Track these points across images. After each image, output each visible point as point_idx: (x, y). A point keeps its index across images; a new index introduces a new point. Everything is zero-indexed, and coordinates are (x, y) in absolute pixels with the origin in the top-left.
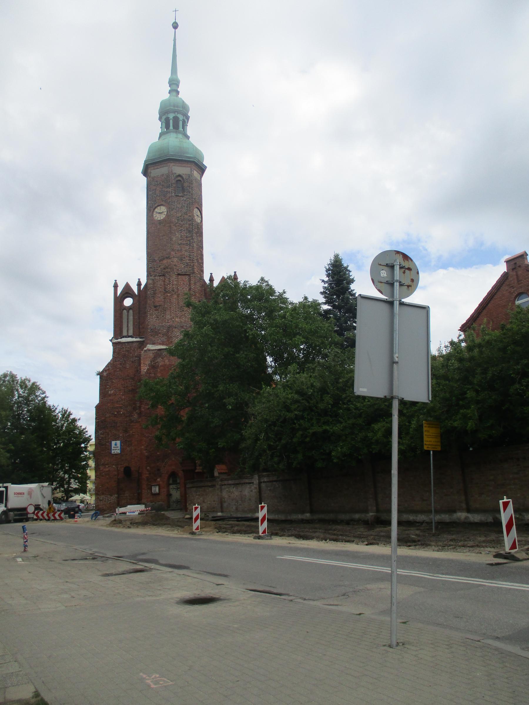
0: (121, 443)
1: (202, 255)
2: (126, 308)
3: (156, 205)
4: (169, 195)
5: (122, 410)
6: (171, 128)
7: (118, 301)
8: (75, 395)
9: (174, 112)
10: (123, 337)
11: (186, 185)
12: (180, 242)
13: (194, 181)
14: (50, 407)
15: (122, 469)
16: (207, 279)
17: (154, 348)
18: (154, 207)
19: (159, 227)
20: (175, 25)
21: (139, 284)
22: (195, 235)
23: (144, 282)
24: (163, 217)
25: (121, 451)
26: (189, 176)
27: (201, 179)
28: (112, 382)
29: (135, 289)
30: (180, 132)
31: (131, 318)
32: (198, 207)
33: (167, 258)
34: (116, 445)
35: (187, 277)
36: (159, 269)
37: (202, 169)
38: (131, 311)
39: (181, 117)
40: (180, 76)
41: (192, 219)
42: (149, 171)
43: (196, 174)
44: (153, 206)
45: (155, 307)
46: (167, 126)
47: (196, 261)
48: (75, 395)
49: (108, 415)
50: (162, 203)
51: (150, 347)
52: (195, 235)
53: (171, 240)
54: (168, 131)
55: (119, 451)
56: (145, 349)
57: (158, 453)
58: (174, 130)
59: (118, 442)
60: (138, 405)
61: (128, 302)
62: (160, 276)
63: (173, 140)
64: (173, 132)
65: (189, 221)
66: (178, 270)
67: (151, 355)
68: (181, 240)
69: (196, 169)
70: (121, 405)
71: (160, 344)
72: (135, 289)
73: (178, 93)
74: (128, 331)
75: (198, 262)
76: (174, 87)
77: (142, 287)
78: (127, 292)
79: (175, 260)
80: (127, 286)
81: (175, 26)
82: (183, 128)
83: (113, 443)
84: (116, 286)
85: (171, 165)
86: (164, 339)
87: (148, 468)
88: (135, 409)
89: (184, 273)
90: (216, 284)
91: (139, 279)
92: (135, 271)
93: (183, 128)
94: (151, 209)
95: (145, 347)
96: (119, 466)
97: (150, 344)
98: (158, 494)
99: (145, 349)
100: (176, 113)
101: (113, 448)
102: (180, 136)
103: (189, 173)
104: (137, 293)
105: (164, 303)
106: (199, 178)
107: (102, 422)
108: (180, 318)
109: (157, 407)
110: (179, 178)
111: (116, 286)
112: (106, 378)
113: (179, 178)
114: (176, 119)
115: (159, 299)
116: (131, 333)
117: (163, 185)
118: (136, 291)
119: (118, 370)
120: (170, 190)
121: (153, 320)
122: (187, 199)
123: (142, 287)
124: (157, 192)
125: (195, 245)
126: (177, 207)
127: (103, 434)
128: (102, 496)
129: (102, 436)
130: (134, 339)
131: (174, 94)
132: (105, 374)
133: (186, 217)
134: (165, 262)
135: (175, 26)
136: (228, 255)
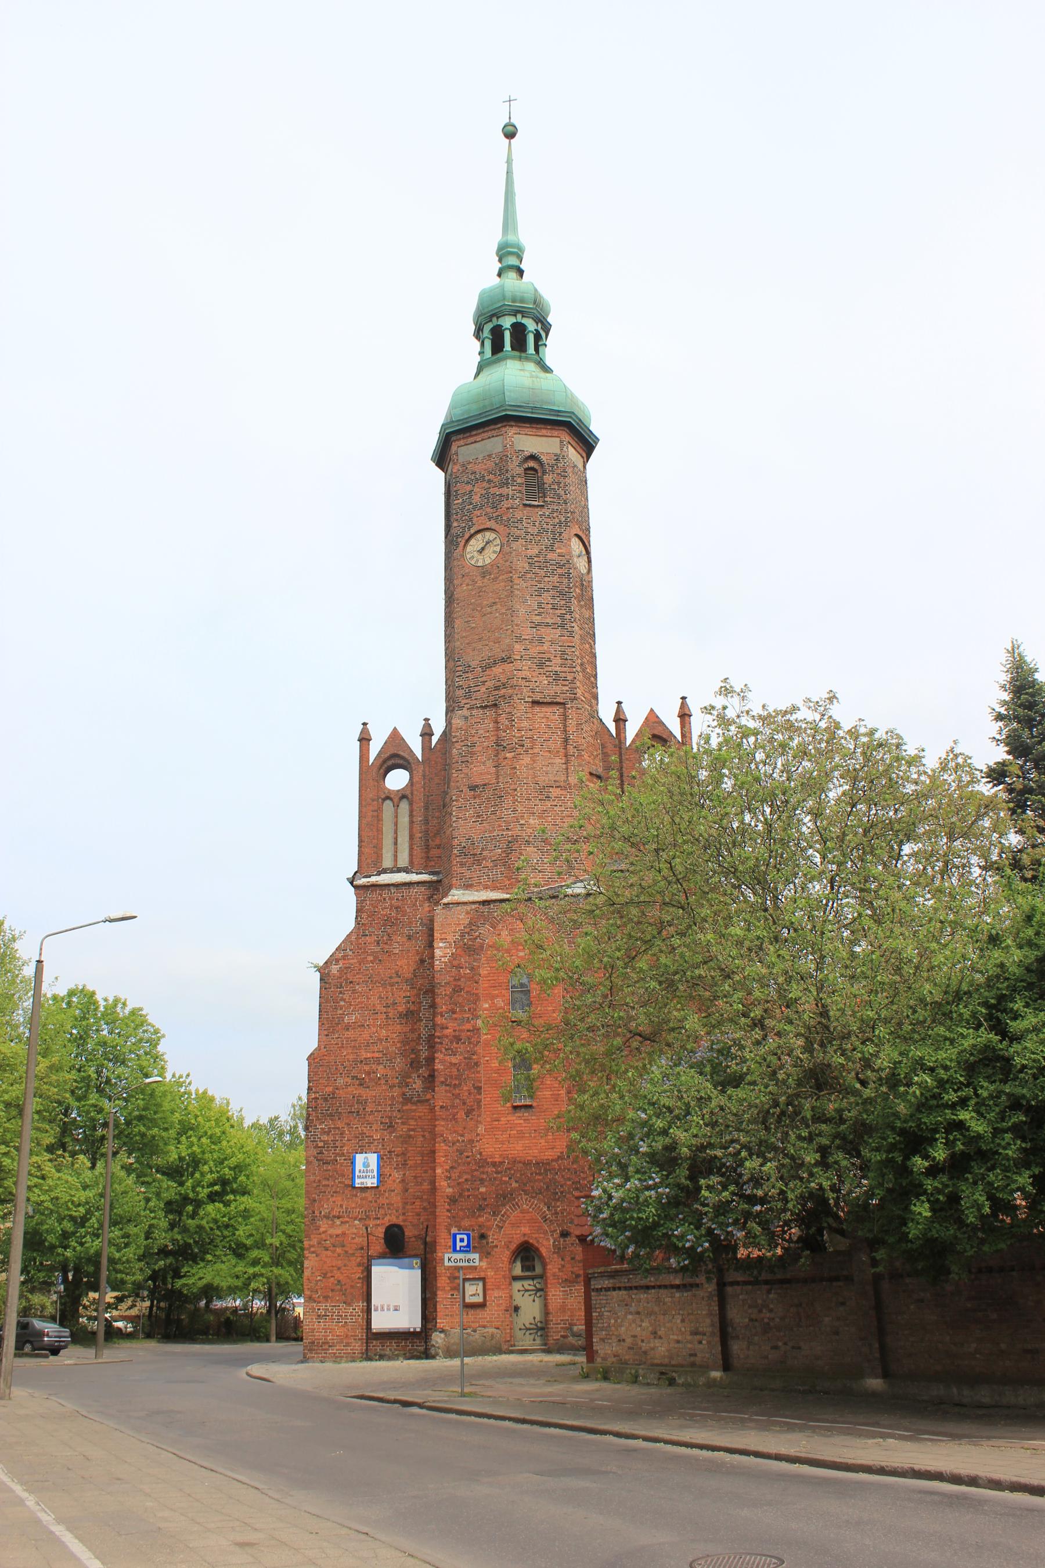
0: (380, 1158)
1: (594, 656)
3: (472, 531)
4: (506, 504)
6: (508, 346)
7: (372, 774)
8: (243, 1042)
9: (515, 313)
10: (385, 871)
11: (548, 479)
12: (537, 619)
13: (569, 470)
14: (653, 723)
15: (380, 1232)
16: (607, 714)
17: (471, 899)
18: (467, 536)
19: (479, 584)
20: (510, 128)
21: (427, 733)
22: (574, 601)
23: (438, 728)
24: (489, 557)
25: (379, 1181)
27: (585, 467)
28: (354, 991)
29: (416, 746)
30: (527, 359)
31: (404, 820)
32: (580, 534)
33: (503, 661)
34: (366, 1165)
35: (553, 714)
36: (483, 689)
37: (587, 444)
38: (404, 806)
39: (531, 325)
40: (525, 236)
41: (565, 565)
42: (454, 448)
43: (573, 455)
44: (463, 533)
45: (473, 788)
46: (497, 347)
47: (578, 668)
48: (243, 1042)
49: (340, 1081)
50: (491, 524)
52: (574, 601)
53: (512, 611)
54: (500, 355)
56: (445, 900)
57: (483, 1190)
58: (517, 353)
59: (373, 1158)
60: (424, 1054)
61: (397, 780)
62: (486, 707)
63: (514, 376)
64: (513, 358)
65: (561, 567)
66: (533, 691)
67: (462, 917)
68: (539, 614)
69: (574, 444)
70: (377, 1055)
71: (486, 888)
72: (416, 746)
73: (520, 272)
74: (396, 856)
75: (584, 670)
76: (512, 261)
77: (435, 739)
78: (395, 756)
80: (395, 737)
81: (510, 133)
82: (537, 350)
83: (360, 1158)
84: (364, 739)
85: (511, 431)
86: (498, 872)
88: (414, 1064)
89: (548, 700)
90: (631, 731)
91: (427, 720)
92: (414, 700)
93: (537, 350)
94: (455, 539)
95: (446, 895)
96: (371, 1223)
97: (460, 887)
98: (482, 1306)
99: (445, 900)
100: (519, 316)
101: (357, 1173)
102: (531, 366)
103: (558, 451)
104: (420, 759)
105: (497, 778)
106: (581, 466)
107: (326, 1100)
108: (540, 817)
109: (948, 1197)
110: (531, 464)
111: (364, 739)
112: (336, 981)
113: (531, 464)
114: (519, 331)
116: (403, 861)
117: (489, 481)
118: (418, 753)
119: (370, 958)
120: (508, 491)
121: (465, 825)
122: (553, 512)
123: (435, 739)
124: (476, 499)
125: (576, 628)
126: (527, 533)
127: (328, 1133)
128: (323, 1306)
129: (325, 1138)
130: (414, 877)
131: (513, 275)
132: (335, 969)
133: (551, 556)
134: (497, 670)
135: (510, 133)
136: (669, 644)
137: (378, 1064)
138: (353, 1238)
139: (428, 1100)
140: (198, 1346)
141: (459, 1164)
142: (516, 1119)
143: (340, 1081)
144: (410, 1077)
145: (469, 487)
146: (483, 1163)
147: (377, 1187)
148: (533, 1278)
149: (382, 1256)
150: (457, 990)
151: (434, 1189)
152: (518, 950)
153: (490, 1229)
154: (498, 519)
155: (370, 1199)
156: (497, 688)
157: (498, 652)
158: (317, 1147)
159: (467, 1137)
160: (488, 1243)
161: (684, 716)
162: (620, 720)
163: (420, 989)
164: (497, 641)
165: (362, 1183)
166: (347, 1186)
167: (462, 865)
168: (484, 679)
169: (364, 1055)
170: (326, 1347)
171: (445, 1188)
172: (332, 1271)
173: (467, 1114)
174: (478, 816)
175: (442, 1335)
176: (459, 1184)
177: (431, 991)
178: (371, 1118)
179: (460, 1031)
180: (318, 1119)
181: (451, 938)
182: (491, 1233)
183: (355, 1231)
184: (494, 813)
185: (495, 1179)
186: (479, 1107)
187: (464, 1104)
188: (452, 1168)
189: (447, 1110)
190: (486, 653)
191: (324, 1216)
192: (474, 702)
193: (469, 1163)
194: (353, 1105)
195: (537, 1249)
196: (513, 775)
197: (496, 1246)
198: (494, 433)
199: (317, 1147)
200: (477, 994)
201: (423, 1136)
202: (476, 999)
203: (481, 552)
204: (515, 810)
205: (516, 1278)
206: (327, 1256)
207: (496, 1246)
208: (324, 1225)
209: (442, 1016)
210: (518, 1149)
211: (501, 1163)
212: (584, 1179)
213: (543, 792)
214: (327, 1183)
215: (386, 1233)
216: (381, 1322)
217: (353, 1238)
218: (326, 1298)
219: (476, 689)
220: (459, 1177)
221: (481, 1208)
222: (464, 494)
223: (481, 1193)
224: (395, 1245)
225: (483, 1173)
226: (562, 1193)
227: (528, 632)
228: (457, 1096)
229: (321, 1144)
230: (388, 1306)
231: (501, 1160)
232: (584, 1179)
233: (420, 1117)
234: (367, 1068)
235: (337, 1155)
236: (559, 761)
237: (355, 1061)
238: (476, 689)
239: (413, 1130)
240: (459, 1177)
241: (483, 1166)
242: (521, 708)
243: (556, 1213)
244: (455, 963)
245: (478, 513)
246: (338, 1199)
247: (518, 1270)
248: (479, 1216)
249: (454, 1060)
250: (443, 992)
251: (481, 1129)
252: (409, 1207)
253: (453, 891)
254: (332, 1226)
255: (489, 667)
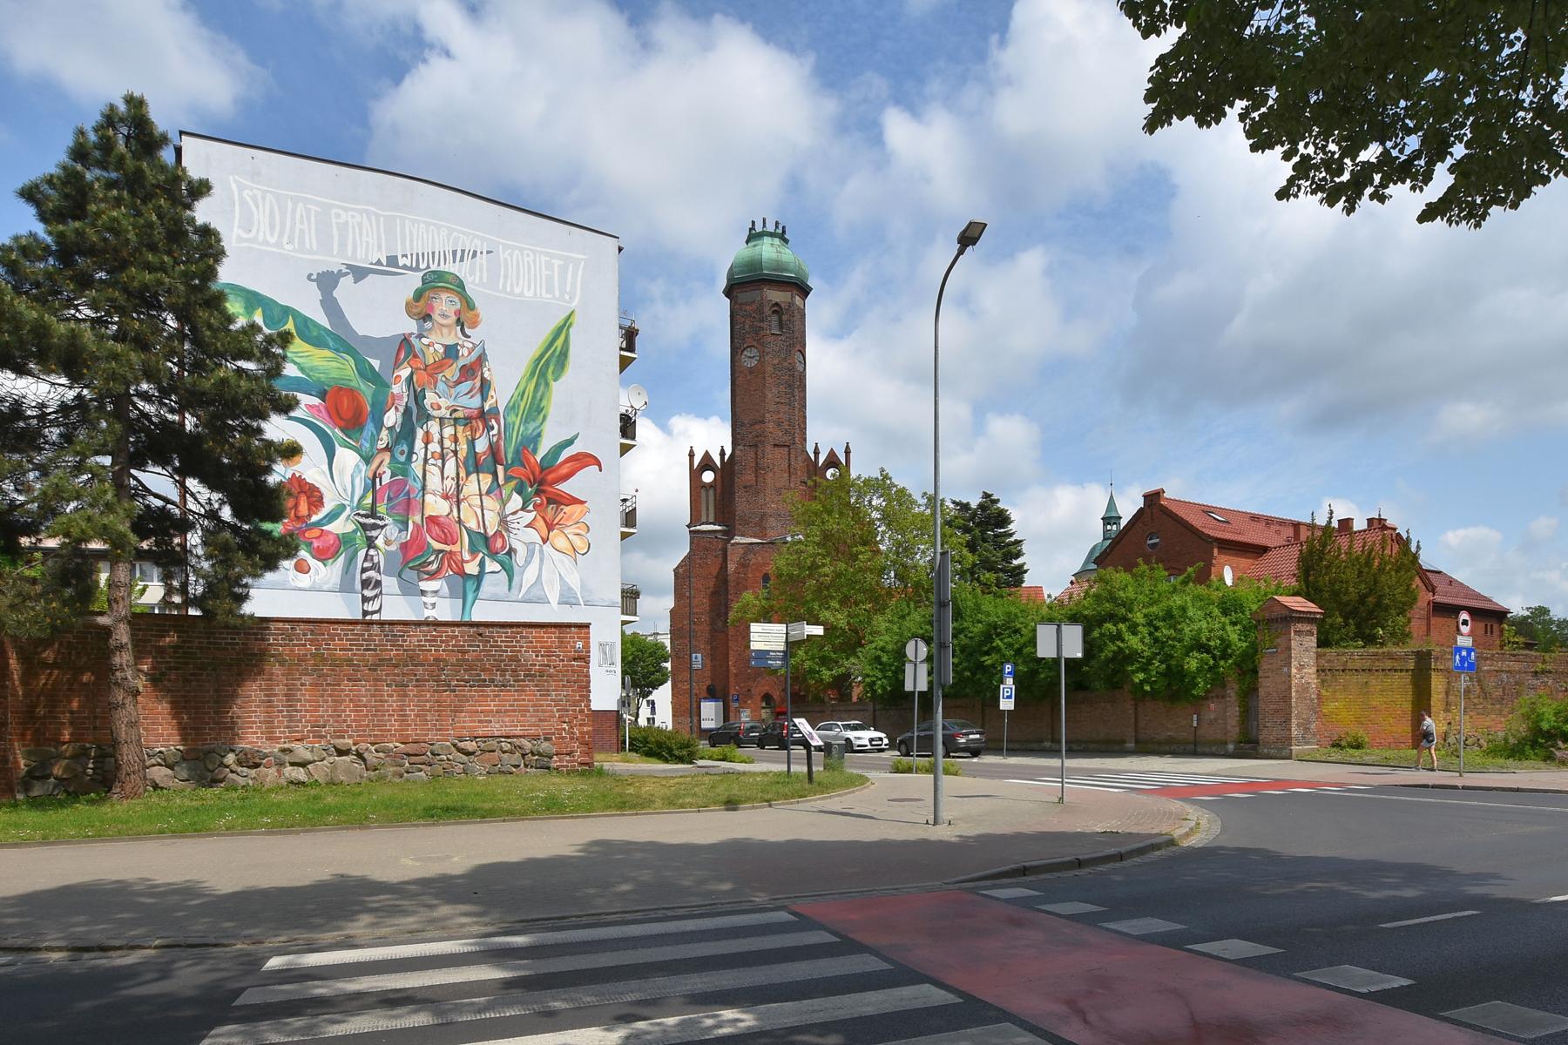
2: (704, 486)
7: (695, 474)
21: (722, 453)
23: (728, 452)
24: (754, 363)
26: (791, 304)
31: (711, 499)
38: (711, 492)
41: (792, 369)
51: (738, 539)
53: (765, 396)
61: (708, 477)
67: (741, 551)
78: (707, 463)
79: (771, 425)
80: (707, 455)
84: (692, 455)
111: (692, 455)
115: (749, 477)
121: (742, 505)
130: (717, 528)
140: (694, 955)
149: (706, 699)
151: (728, 670)
154: (758, 341)
161: (847, 452)
162: (817, 453)
171: (733, 670)
177: (726, 581)
203: (750, 360)
213: (779, 491)
216: (705, 725)
224: (712, 695)
227: (772, 407)
242: (769, 448)
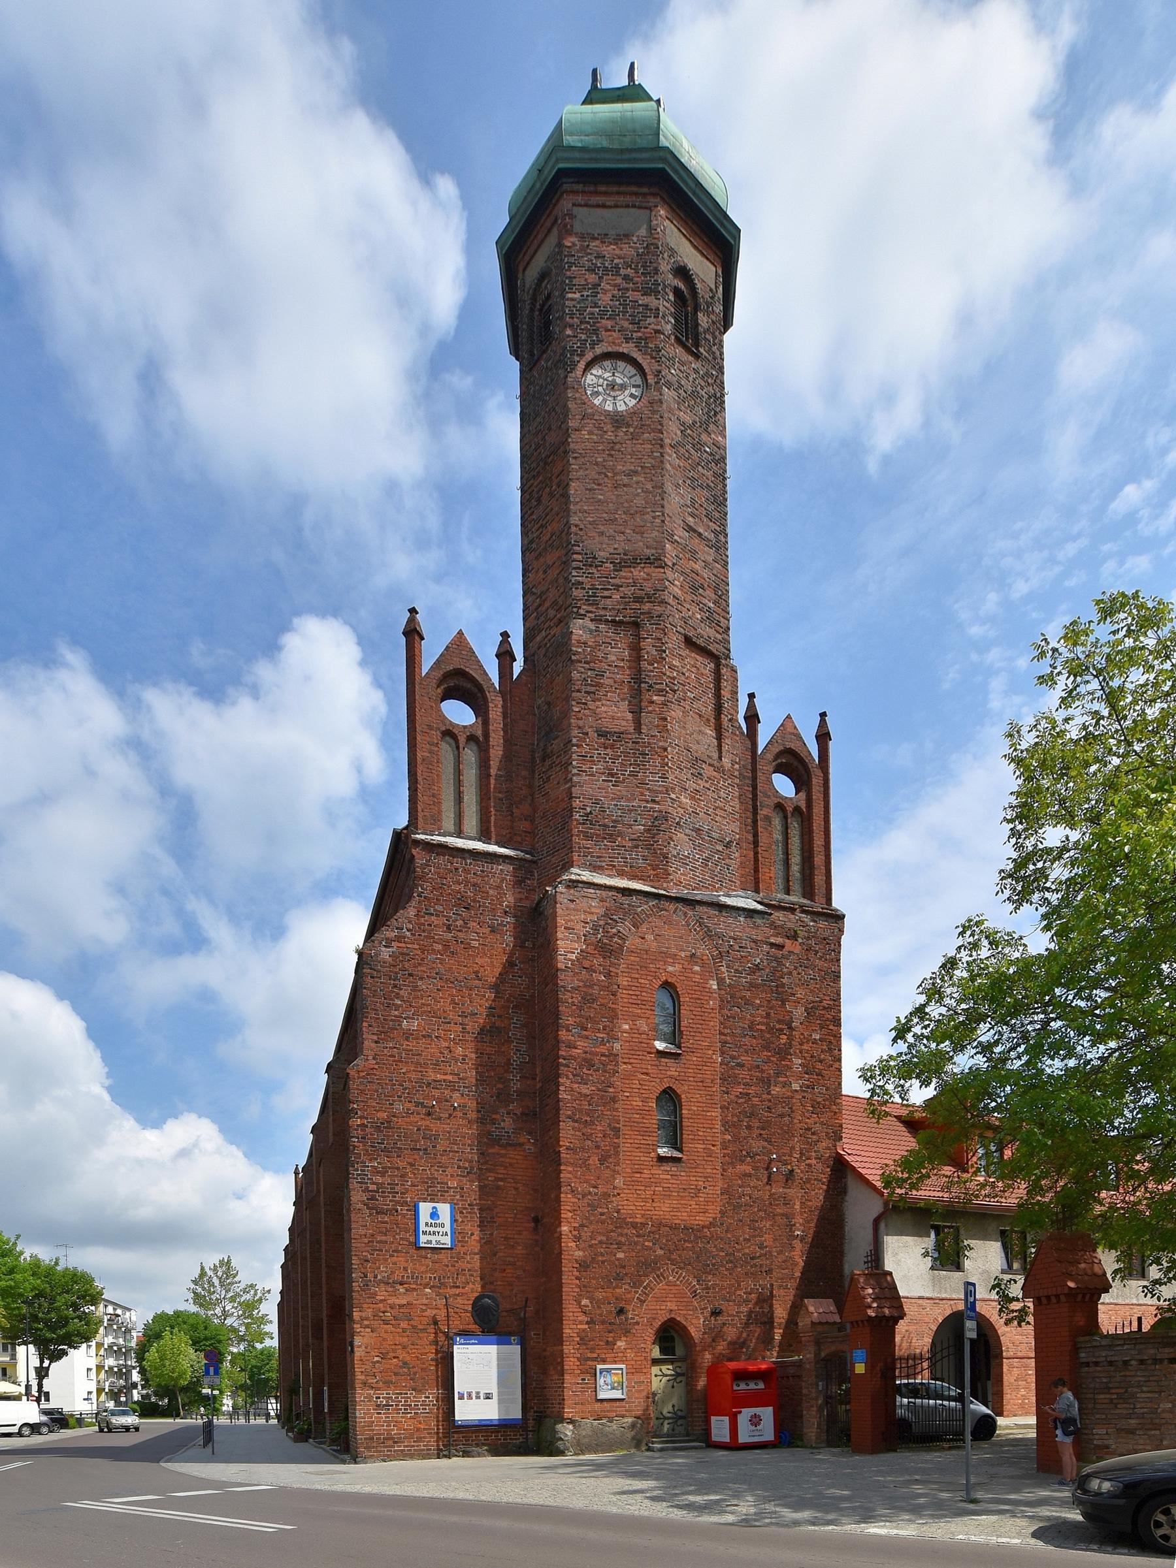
3: (599, 350)
5: (456, 1095)
19: (610, 436)
21: (505, 655)
28: (415, 988)
31: (470, 775)
33: (648, 561)
34: (434, 1215)
36: (616, 597)
42: (566, 204)
45: (602, 734)
55: (447, 1241)
57: (620, 1255)
59: (444, 1209)
62: (621, 622)
67: (595, 906)
70: (450, 1078)
86: (638, 858)
87: (584, 1302)
101: (422, 1227)
111: (412, 633)
117: (626, 278)
119: (439, 947)
124: (605, 299)
134: (638, 573)
137: (453, 1090)
138: (424, 1311)
139: (521, 1145)
141: (591, 1223)
142: (663, 1173)
143: (399, 1107)
144: (497, 1113)
145: (592, 278)
146: (621, 1223)
147: (451, 1249)
148: (672, 1362)
149: (465, 1334)
150: (588, 999)
152: (665, 963)
153: (628, 1301)
155: (446, 1261)
156: (638, 600)
157: (639, 546)
158: (367, 1190)
159: (601, 1189)
160: (626, 1319)
161: (823, 737)
163: (508, 1001)
164: (639, 531)
165: (430, 1242)
166: (410, 1243)
167: (588, 837)
168: (617, 581)
169: (432, 1075)
170: (390, 1443)
172: (394, 1351)
173: (603, 1160)
174: (612, 775)
175: (571, 1427)
176: (590, 1246)
178: (444, 1159)
179: (591, 1053)
180: (367, 1153)
181: (581, 930)
182: (630, 1308)
183: (426, 1302)
184: (633, 774)
185: (636, 1243)
186: (617, 1153)
187: (598, 1147)
188: (582, 1226)
189: (575, 1153)
190: (620, 545)
191: (381, 1281)
192: (602, 613)
193: (603, 1222)
194: (418, 1141)
195: (684, 1328)
196: (664, 729)
197: (637, 1323)
198: (638, 200)
199: (367, 1190)
200: (613, 1010)
201: (516, 1189)
202: (613, 1016)
204: (664, 777)
205: (655, 1362)
206: (386, 1332)
207: (637, 1323)
208: (382, 1293)
209: (568, 1030)
210: (664, 1210)
211: (644, 1225)
212: (739, 1251)
214: (384, 1238)
215: (474, 1305)
216: (466, 1411)
217: (424, 1311)
218: (388, 1384)
219: (606, 593)
220: (592, 1238)
221: (619, 1278)
222: (583, 288)
223: (618, 1259)
225: (622, 1235)
226: (714, 1265)
228: (588, 1137)
229: (372, 1187)
230: (478, 1393)
231: (643, 1220)
232: (739, 1251)
233: (511, 1164)
234: (436, 1093)
235: (398, 1202)
236: (710, 732)
237: (420, 1082)
238: (606, 593)
239: (501, 1180)
240: (592, 1238)
241: (621, 1227)
243: (708, 1288)
244: (586, 964)
245: (609, 324)
246: (401, 1261)
247: (656, 1353)
248: (617, 1287)
249: (585, 1090)
250: (568, 1001)
251: (619, 1182)
252: (497, 1274)
253: (573, 870)
254: (395, 1293)
255: (619, 566)
